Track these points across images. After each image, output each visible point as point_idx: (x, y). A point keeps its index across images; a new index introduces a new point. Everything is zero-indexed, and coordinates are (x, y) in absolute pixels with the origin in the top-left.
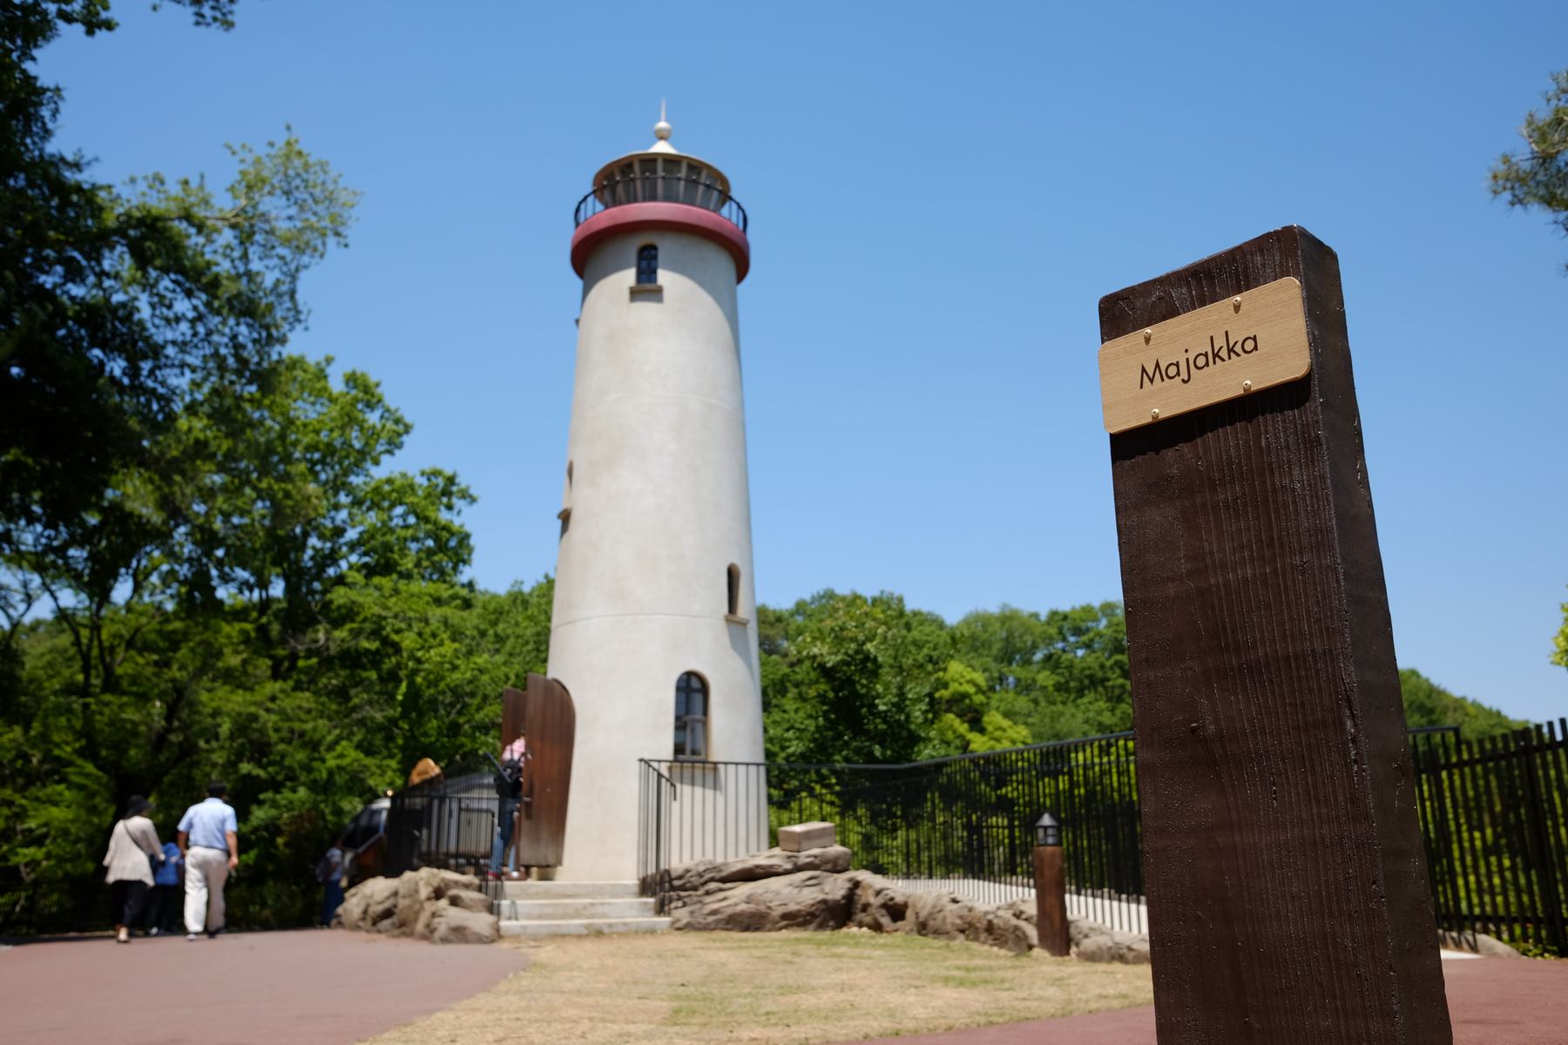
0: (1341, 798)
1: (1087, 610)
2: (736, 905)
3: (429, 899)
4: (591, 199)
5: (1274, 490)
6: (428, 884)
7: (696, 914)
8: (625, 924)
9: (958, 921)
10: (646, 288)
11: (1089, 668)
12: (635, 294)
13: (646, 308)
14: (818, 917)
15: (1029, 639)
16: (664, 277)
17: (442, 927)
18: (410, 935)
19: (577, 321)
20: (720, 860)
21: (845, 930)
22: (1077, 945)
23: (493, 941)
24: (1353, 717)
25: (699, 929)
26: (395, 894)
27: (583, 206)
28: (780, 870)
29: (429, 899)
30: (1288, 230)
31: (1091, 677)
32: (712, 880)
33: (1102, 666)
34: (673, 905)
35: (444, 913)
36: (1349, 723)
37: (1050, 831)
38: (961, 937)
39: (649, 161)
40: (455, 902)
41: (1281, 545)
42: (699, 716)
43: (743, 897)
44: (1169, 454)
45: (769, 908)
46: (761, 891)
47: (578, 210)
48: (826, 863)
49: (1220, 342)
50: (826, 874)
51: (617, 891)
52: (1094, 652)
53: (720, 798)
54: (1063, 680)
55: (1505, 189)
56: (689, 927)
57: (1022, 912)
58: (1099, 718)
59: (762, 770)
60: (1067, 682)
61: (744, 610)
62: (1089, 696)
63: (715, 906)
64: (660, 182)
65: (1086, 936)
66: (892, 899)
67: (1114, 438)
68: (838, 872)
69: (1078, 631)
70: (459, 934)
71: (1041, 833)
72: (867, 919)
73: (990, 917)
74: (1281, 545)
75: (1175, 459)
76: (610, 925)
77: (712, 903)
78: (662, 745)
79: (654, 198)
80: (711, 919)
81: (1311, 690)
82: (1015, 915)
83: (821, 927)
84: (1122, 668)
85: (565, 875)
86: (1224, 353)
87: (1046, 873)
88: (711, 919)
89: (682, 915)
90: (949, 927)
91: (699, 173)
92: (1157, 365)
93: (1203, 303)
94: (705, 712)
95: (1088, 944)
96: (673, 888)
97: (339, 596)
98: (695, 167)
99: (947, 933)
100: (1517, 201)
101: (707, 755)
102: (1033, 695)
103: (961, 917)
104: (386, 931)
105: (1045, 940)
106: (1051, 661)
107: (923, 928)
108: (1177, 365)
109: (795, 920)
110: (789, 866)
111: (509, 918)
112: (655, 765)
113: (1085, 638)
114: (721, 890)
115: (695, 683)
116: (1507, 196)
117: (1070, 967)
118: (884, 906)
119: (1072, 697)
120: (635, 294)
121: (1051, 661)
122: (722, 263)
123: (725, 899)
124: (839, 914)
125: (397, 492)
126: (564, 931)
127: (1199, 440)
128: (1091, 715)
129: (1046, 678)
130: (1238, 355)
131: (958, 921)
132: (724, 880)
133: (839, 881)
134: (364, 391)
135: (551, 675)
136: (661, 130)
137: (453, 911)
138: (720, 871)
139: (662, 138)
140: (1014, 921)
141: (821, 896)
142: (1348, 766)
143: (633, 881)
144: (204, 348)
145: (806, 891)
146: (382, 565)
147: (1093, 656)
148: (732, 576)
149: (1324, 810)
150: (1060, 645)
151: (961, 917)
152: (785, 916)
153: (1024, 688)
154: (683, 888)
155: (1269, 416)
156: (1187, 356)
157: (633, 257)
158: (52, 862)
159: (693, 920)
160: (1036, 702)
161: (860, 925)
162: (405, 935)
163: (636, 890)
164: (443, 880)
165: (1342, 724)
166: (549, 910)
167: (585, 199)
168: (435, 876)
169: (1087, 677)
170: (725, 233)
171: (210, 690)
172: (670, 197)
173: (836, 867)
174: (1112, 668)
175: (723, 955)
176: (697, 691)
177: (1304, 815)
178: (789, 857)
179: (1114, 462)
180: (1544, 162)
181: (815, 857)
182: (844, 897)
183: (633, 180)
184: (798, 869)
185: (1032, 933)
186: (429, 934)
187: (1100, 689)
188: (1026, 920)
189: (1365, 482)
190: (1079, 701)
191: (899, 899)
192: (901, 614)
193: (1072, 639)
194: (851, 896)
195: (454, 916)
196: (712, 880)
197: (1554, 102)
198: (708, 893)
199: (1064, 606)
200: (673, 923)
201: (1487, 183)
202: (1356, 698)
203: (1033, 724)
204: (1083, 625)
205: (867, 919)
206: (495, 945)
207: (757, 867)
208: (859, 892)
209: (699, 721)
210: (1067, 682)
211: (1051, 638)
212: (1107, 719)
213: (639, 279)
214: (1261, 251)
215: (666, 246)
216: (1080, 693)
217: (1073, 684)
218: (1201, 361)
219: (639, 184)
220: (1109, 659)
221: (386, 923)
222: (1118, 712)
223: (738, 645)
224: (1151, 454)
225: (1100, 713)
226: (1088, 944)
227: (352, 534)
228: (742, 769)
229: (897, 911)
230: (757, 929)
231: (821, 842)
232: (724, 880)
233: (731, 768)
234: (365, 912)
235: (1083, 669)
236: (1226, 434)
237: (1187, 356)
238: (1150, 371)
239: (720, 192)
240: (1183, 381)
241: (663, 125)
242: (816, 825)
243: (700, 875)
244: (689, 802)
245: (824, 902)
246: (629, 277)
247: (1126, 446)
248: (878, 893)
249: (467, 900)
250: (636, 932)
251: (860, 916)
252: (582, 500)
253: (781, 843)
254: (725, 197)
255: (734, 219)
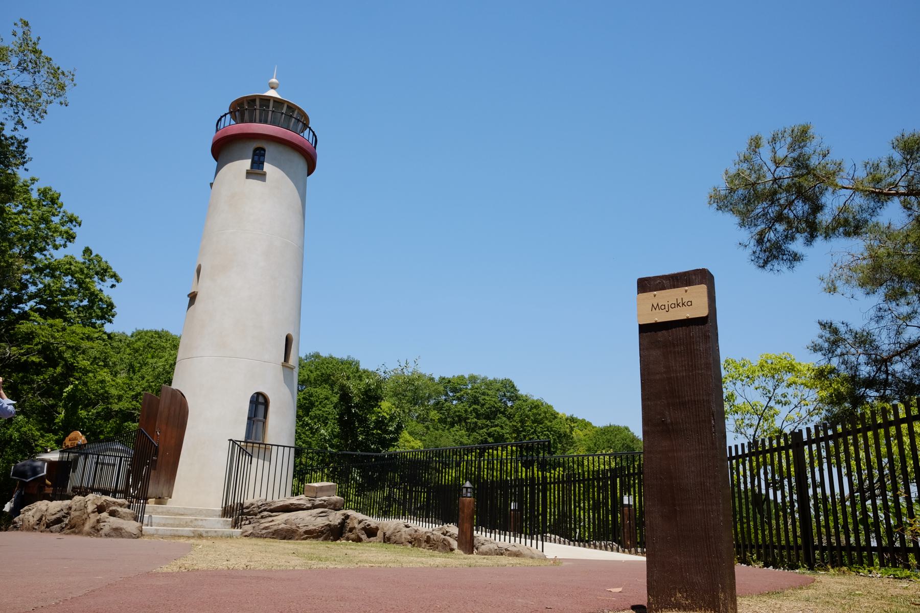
0: (709, 443)
1: (462, 378)
2: (279, 525)
3: (93, 512)
4: (228, 116)
5: (694, 350)
6: (93, 503)
7: (256, 528)
8: (216, 532)
9: (409, 537)
10: (256, 172)
11: (459, 411)
12: (249, 174)
13: (254, 183)
14: (325, 533)
15: (427, 392)
16: (267, 167)
17: (106, 529)
18: (80, 533)
19: (211, 184)
20: (269, 499)
21: (338, 542)
22: (477, 549)
23: (138, 537)
24: (714, 419)
25: (258, 537)
26: (70, 508)
27: (223, 119)
28: (305, 507)
29: (93, 512)
30: (704, 270)
31: (459, 416)
32: (265, 510)
33: (466, 411)
34: (243, 523)
35: (107, 520)
36: (713, 421)
37: (469, 490)
38: (409, 546)
39: (266, 100)
40: (113, 514)
41: (695, 367)
42: (261, 417)
43: (283, 521)
44: (660, 333)
45: (298, 527)
46: (293, 518)
47: (220, 120)
48: (330, 505)
50: (330, 510)
51: (209, 513)
52: (462, 402)
53: (267, 463)
54: (444, 417)
55: (714, 202)
56: (252, 535)
57: (447, 532)
58: (461, 440)
59: (293, 450)
60: (446, 418)
61: (293, 361)
62: (457, 427)
63: (267, 525)
64: (270, 113)
65: (483, 544)
66: (369, 525)
67: (640, 326)
68: (336, 510)
69: (455, 390)
70: (117, 532)
71: (464, 490)
72: (353, 536)
73: (428, 534)
74: (695, 367)
75: (662, 335)
76: (207, 532)
77: (265, 523)
78: (240, 435)
79: (266, 122)
80: (264, 531)
81: (701, 411)
82: (442, 534)
83: (326, 539)
84: (476, 413)
85: (173, 503)
86: (681, 305)
87: (465, 511)
88: (264, 531)
89: (248, 528)
90: (403, 540)
91: (293, 112)
92: (658, 305)
93: (674, 287)
94: (265, 416)
95: (483, 548)
96: (243, 514)
97: (24, 327)
98: (292, 108)
99: (402, 543)
100: (719, 208)
101: (263, 441)
102: (426, 424)
103: (410, 535)
104: (56, 532)
105: (460, 546)
106: (438, 406)
107: (387, 540)
109: (312, 534)
110: (309, 505)
111: (147, 525)
112: (239, 443)
113: (458, 394)
114: (270, 516)
115: (261, 400)
116: (715, 205)
117: (474, 558)
118: (364, 529)
119: (447, 427)
120: (249, 174)
121: (438, 406)
122: (300, 164)
123: (273, 521)
124: (335, 533)
125: (67, 269)
126: (180, 533)
127: (670, 331)
128: (457, 438)
129: (434, 415)
131: (409, 537)
132: (272, 511)
133: (338, 515)
134: (50, 199)
135: (174, 386)
136: (273, 83)
137: (112, 519)
138: (271, 506)
139: (272, 88)
140: (443, 536)
141: (327, 522)
142: (712, 434)
143: (218, 507)
145: (319, 519)
146: (52, 310)
147: (462, 405)
148: (288, 341)
149: (703, 447)
150: (444, 398)
151: (410, 535)
152: (306, 532)
153: (422, 420)
154: (248, 514)
155: (694, 326)
157: (251, 153)
159: (254, 532)
160: (428, 428)
161: (348, 539)
162: (74, 533)
163: (220, 513)
164: (105, 501)
165: (711, 421)
166: (171, 522)
167: (225, 115)
168: (97, 498)
169: (457, 416)
170: (308, 150)
172: (273, 123)
173: (336, 507)
174: (471, 412)
175: (296, 547)
176: (261, 404)
177: (697, 448)
178: (310, 500)
179: (640, 333)
180: (731, 192)
181: (325, 501)
182: (339, 524)
183: (255, 109)
184: (314, 507)
185: (455, 544)
186: (96, 530)
187: (464, 424)
188: (450, 536)
189: (718, 350)
190: (451, 430)
191: (373, 525)
192: (358, 371)
193: (451, 394)
194: (343, 523)
195: (114, 522)
196: (265, 510)
197: (737, 165)
198: (262, 517)
199: (449, 375)
200: (243, 533)
201: (707, 200)
202: (715, 414)
203: (425, 440)
204: (458, 387)
205: (353, 536)
206: (139, 539)
207: (292, 504)
208: (348, 521)
209: (260, 421)
210: (446, 418)
211: (440, 393)
212: (465, 440)
213: (252, 166)
214: (695, 275)
215: (271, 150)
216: (452, 425)
217: (449, 420)
218: (673, 306)
219: (258, 112)
220: (469, 407)
221: (57, 527)
222: (472, 438)
223: (287, 380)
224: (653, 333)
225: (461, 437)
226: (483, 548)
227: (32, 289)
228: (281, 449)
229: (371, 532)
230: (290, 539)
231: (329, 493)
232: (272, 511)
233: (275, 448)
234: (40, 520)
235: (455, 412)
236: (679, 330)
238: (655, 306)
239: (303, 123)
241: (274, 80)
242: (325, 484)
243: (259, 507)
244: (256, 467)
245: (329, 525)
246: (246, 164)
247: (644, 329)
248: (360, 522)
249: (121, 513)
250: (221, 537)
251: (348, 534)
252: (204, 289)
253: (305, 493)
254: (306, 126)
255: (310, 141)
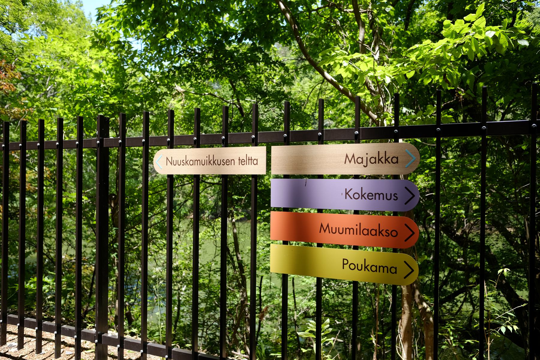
49: (211, 158)
86: (383, 160)
92: (353, 156)
108: (362, 158)
130: (389, 163)
144: (273, 87)
156: (367, 156)
158: (292, 242)
171: (71, 256)
237: (367, 156)
240: (364, 166)
